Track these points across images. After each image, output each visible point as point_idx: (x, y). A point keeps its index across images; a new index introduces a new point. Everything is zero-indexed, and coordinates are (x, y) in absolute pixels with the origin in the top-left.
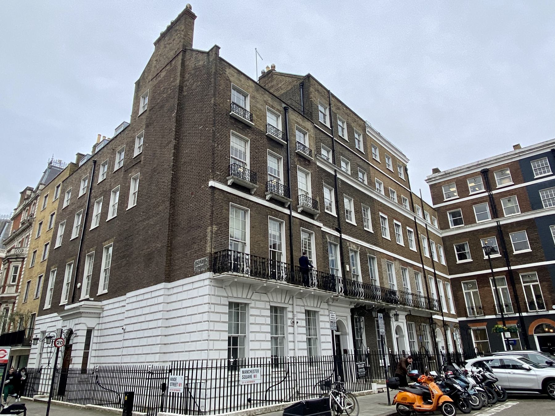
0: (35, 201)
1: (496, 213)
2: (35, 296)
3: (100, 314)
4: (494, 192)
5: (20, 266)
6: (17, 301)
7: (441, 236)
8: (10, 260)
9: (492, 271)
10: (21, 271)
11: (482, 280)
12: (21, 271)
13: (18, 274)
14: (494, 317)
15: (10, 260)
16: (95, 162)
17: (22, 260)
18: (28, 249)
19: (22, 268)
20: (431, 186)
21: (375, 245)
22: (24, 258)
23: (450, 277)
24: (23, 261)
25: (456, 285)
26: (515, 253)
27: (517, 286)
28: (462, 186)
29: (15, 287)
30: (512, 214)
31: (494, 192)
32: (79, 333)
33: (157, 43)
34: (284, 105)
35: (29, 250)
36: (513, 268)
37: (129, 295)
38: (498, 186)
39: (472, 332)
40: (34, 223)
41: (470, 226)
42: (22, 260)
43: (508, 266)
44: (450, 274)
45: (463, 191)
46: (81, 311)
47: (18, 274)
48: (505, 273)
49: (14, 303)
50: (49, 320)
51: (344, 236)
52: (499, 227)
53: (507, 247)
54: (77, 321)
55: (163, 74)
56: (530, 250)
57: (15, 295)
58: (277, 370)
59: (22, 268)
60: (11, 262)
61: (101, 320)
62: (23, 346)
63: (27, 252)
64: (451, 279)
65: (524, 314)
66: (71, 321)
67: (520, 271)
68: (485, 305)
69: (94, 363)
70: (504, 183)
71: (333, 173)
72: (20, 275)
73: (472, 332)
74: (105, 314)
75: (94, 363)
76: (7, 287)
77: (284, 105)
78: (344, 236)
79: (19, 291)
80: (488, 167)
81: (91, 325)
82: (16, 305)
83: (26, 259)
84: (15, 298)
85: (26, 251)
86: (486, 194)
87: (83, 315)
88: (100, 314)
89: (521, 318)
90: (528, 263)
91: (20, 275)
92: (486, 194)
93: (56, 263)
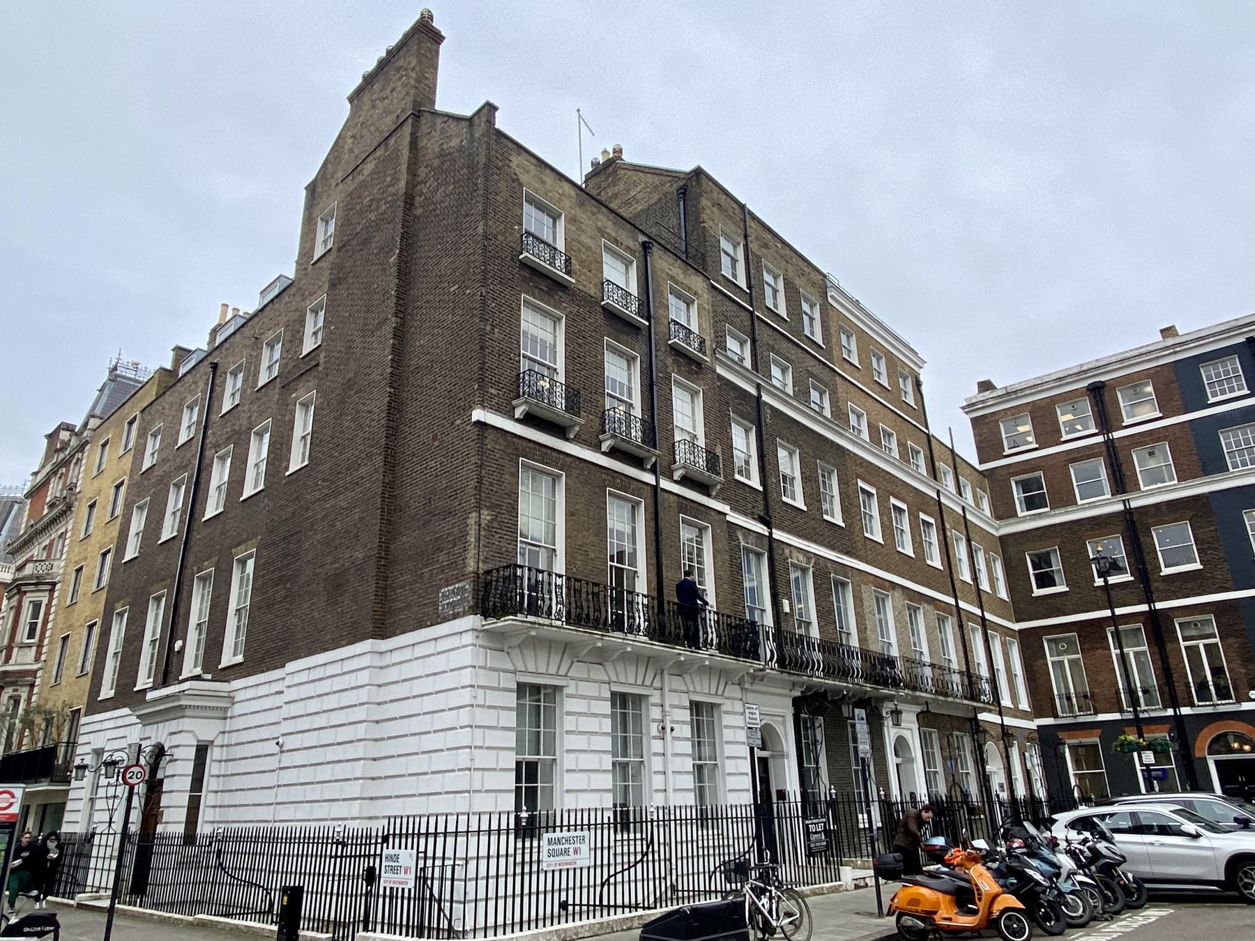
0: (80, 455)
1: (1121, 482)
2: (79, 670)
3: (226, 709)
4: (1117, 435)
5: (45, 601)
6: (38, 681)
7: (997, 534)
8: (24, 589)
9: (1113, 612)
10: (47, 614)
11: (1091, 634)
12: (47, 614)
13: (40, 621)
14: (1116, 716)
15: (24, 589)
16: (215, 367)
17: (49, 587)
18: (63, 564)
19: (49, 605)
20: (975, 422)
21: (848, 553)
22: (54, 584)
23: (1017, 626)
24: (52, 591)
25: (1030, 644)
26: (1166, 571)
27: (1169, 646)
28: (1044, 420)
29: (34, 649)
30: (1158, 485)
31: (1117, 435)
32: (178, 753)
33: (355, 97)
34: (642, 238)
35: (66, 566)
36: (1159, 605)
37: (291, 666)
38: (1127, 422)
39: (1067, 750)
40: (76, 503)
41: (1062, 511)
42: (49, 587)
43: (1150, 601)
44: (1018, 621)
45: (1047, 432)
46: (183, 703)
47: (40, 621)
48: (1142, 618)
49: (32, 686)
50: (111, 724)
51: (777, 534)
52: (1128, 513)
53: (1147, 558)
54: (173, 725)
55: (369, 167)
56: (1198, 566)
57: (35, 667)
58: (625, 837)
59: (49, 605)
60: (25, 592)
61: (229, 725)
62: (52, 782)
63: (61, 571)
64: (1020, 631)
65: (1185, 711)
66: (161, 725)
67: (1176, 613)
68: (1097, 691)
69: (212, 822)
70: (1140, 415)
71: (753, 391)
72: (46, 622)
73: (1067, 750)
74: (238, 710)
75: (212, 822)
76: (15, 650)
77: (642, 238)
78: (777, 534)
79: (43, 657)
80: (1103, 379)
81: (205, 736)
82: (36, 690)
83: (58, 587)
84: (34, 673)
85: (59, 567)
86: (1100, 439)
87: (188, 712)
88: (226, 709)
89: (1178, 719)
90: (1194, 596)
91: (46, 622)
92: (1100, 439)
93: (128, 595)
